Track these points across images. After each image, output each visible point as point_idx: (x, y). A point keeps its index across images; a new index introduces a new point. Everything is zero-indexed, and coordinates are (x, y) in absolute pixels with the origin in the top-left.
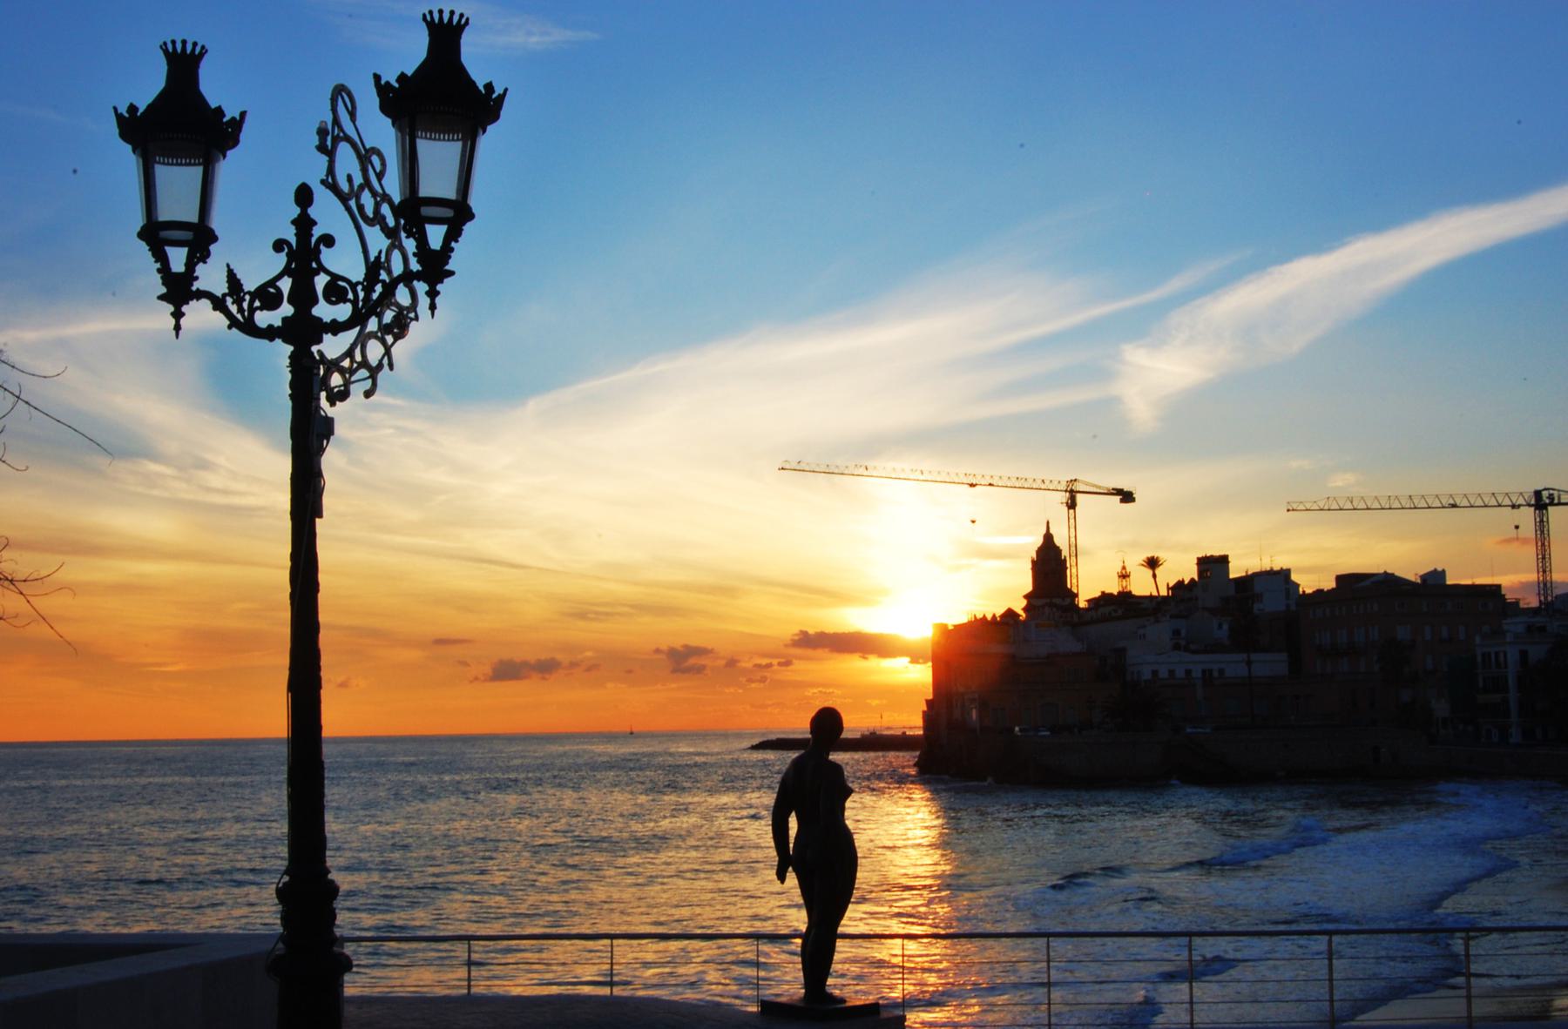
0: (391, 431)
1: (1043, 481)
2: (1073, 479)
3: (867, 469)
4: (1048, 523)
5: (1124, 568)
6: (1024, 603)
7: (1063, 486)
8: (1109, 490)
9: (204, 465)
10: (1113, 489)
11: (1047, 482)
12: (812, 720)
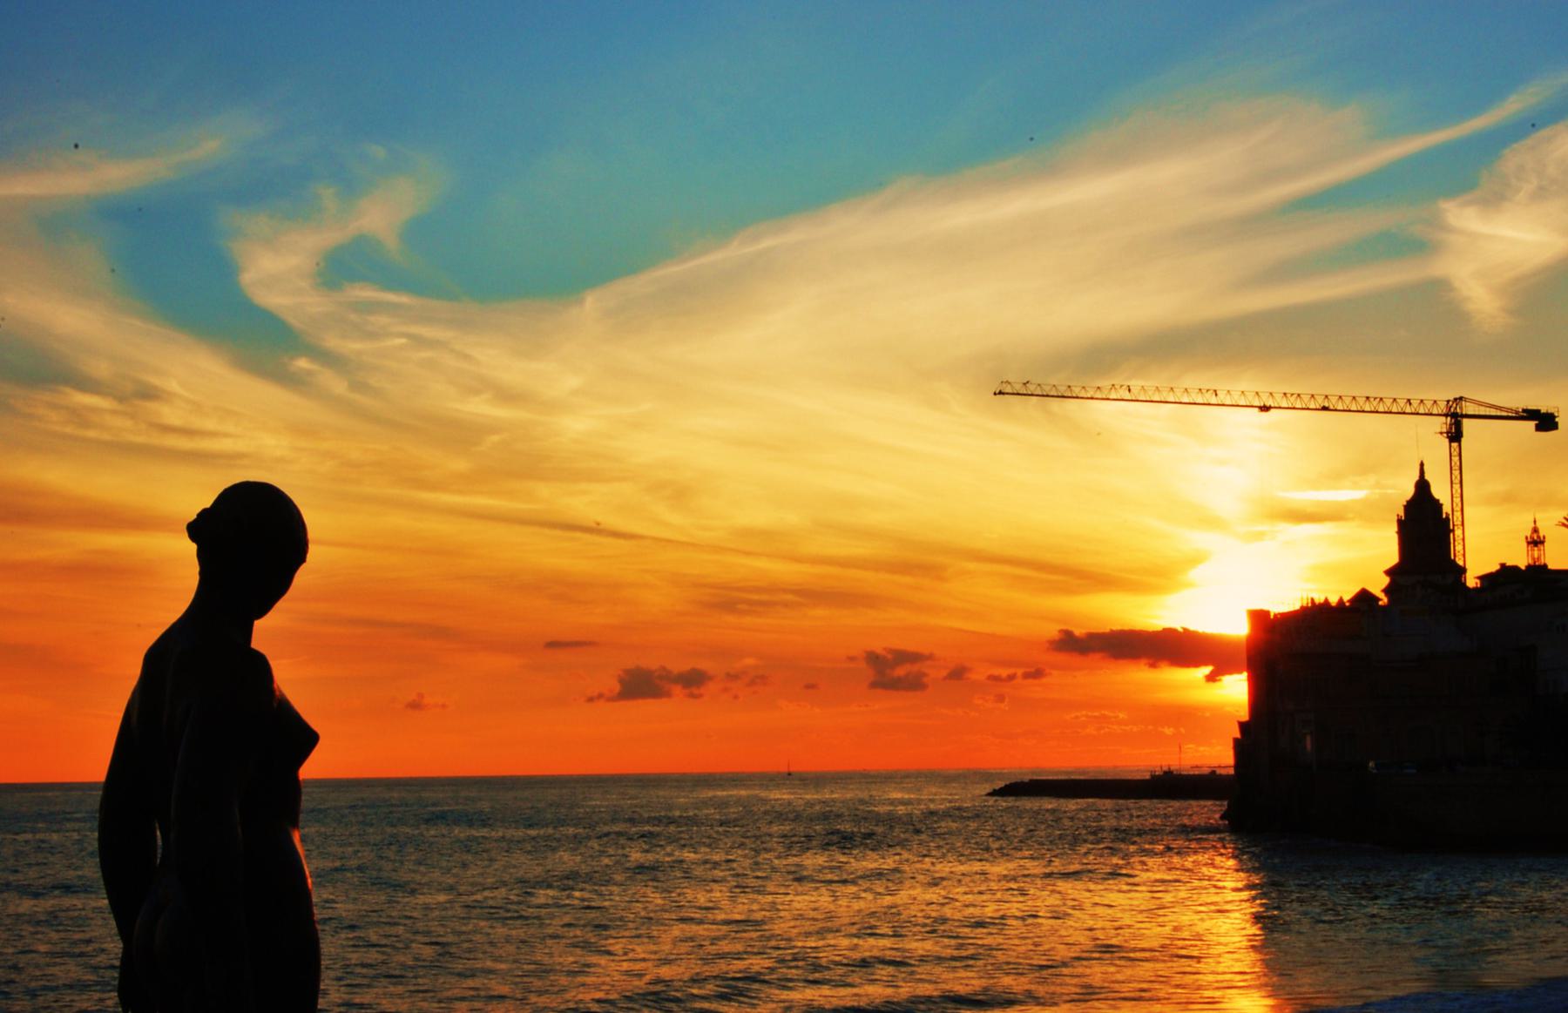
0: (403, 341)
1: (1409, 400)
2: (1458, 396)
3: (1129, 390)
4: (1422, 465)
5: (1535, 530)
6: (1386, 580)
7: (1442, 408)
8: (1517, 412)
9: (150, 394)
10: (1524, 411)
11: (1415, 403)
12: (146, 656)
